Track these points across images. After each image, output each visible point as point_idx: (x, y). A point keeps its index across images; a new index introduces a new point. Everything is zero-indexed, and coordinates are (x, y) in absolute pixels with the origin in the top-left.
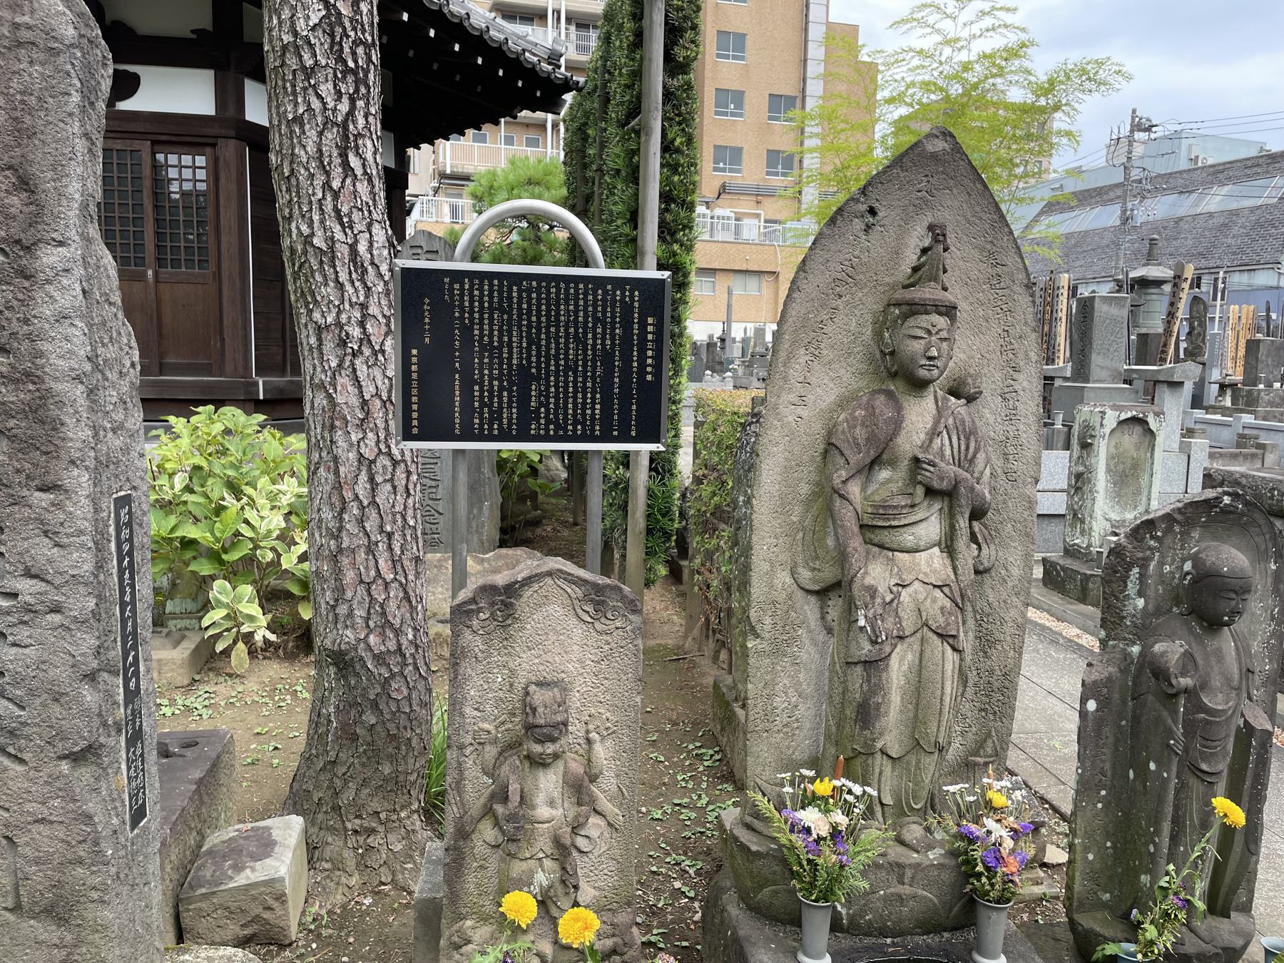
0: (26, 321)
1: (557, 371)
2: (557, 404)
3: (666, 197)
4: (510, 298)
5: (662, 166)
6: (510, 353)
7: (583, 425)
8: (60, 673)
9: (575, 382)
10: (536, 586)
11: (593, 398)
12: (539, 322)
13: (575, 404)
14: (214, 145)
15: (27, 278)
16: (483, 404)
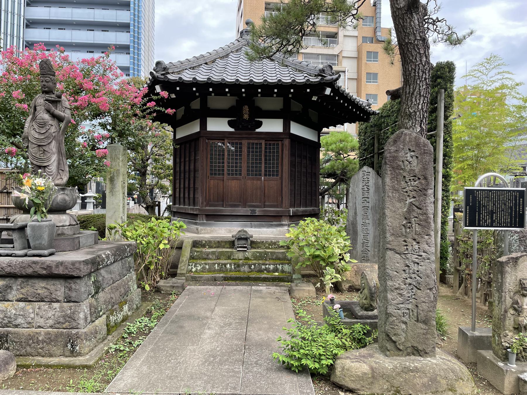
0: (425, 203)
1: (500, 211)
2: (499, 219)
3: (445, 155)
4: (489, 195)
5: (443, 146)
6: (489, 207)
7: (506, 223)
8: (429, 272)
9: (504, 214)
10: (523, 258)
11: (508, 217)
12: (496, 200)
13: (504, 219)
14: (282, 141)
15: (425, 195)
16: (483, 219)
